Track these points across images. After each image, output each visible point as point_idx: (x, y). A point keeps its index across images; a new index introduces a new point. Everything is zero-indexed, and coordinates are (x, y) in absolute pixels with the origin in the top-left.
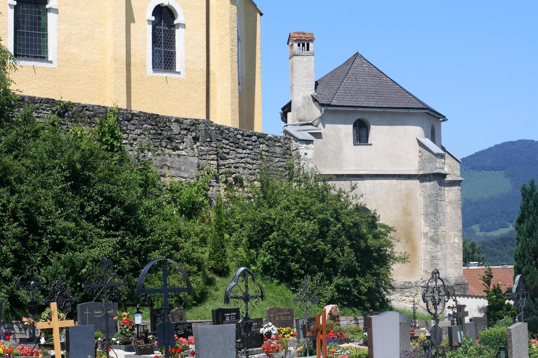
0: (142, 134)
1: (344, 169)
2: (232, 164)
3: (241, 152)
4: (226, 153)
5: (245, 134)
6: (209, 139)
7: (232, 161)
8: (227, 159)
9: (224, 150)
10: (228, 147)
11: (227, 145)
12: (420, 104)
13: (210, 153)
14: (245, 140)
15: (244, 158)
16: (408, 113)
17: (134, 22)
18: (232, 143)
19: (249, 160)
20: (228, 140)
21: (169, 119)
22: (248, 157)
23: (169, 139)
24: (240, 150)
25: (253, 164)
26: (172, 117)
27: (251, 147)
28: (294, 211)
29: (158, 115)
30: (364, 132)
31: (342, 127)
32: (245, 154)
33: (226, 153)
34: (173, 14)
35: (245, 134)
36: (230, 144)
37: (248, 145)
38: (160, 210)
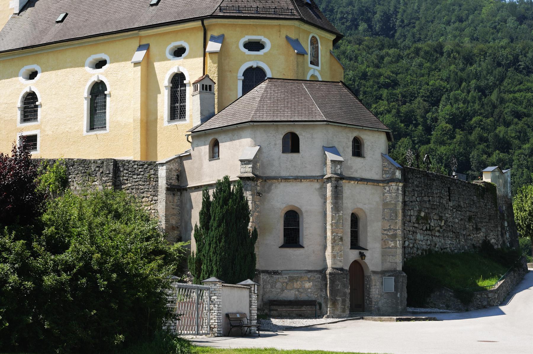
1: (203, 181)
2: (130, 187)
4: (125, 180)
5: (139, 164)
6: (108, 172)
7: (129, 185)
8: (126, 184)
9: (125, 178)
10: (127, 175)
11: (126, 173)
13: (107, 181)
14: (139, 168)
15: (137, 181)
16: (261, 125)
17: (160, 93)
18: (130, 172)
19: (140, 183)
20: (128, 170)
21: (90, 161)
22: (140, 181)
23: (89, 175)
24: (135, 177)
25: (144, 185)
26: (92, 160)
27: (142, 173)
29: (86, 160)
30: (216, 149)
31: (203, 148)
32: (139, 178)
33: (125, 180)
34: (174, 77)
35: (139, 164)
36: (130, 173)
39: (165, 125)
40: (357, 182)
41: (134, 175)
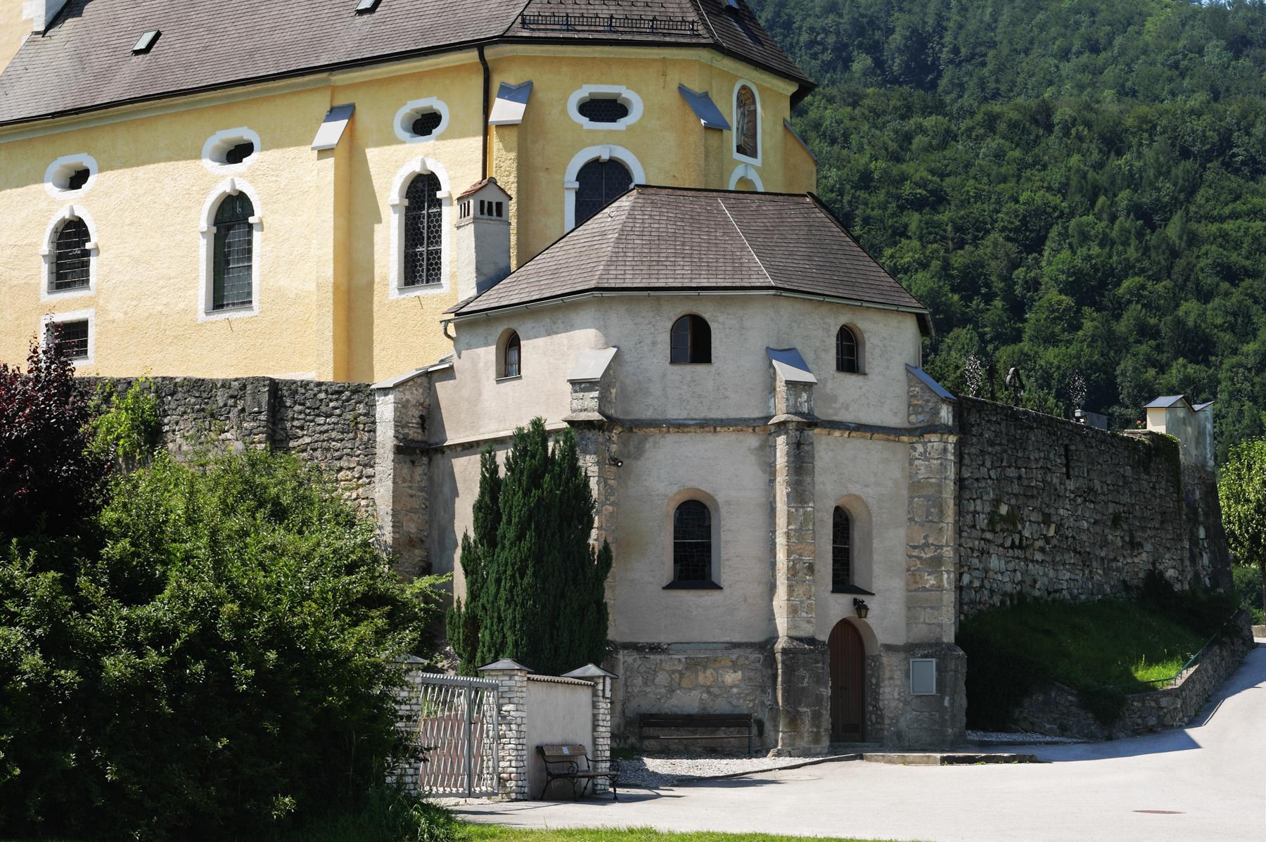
0: (185, 413)
1: (481, 431)
2: (308, 444)
3: (322, 422)
4: (297, 427)
5: (330, 391)
6: (256, 409)
7: (307, 440)
8: (299, 438)
9: (296, 423)
10: (302, 416)
11: (300, 413)
12: (566, 680)
13: (255, 431)
14: (331, 401)
15: (326, 431)
16: (621, 297)
18: (308, 408)
19: (334, 434)
20: (303, 404)
21: (213, 383)
22: (333, 430)
23: (212, 415)
24: (321, 420)
25: (342, 440)
26: (218, 380)
27: (338, 412)
28: (1020, 100)
30: (514, 355)
31: (481, 351)
32: (329, 424)
33: (297, 427)
34: (413, 182)
35: (330, 391)
36: (308, 411)
37: (335, 408)
38: (1120, 163)
39: (391, 298)
41: (318, 415)
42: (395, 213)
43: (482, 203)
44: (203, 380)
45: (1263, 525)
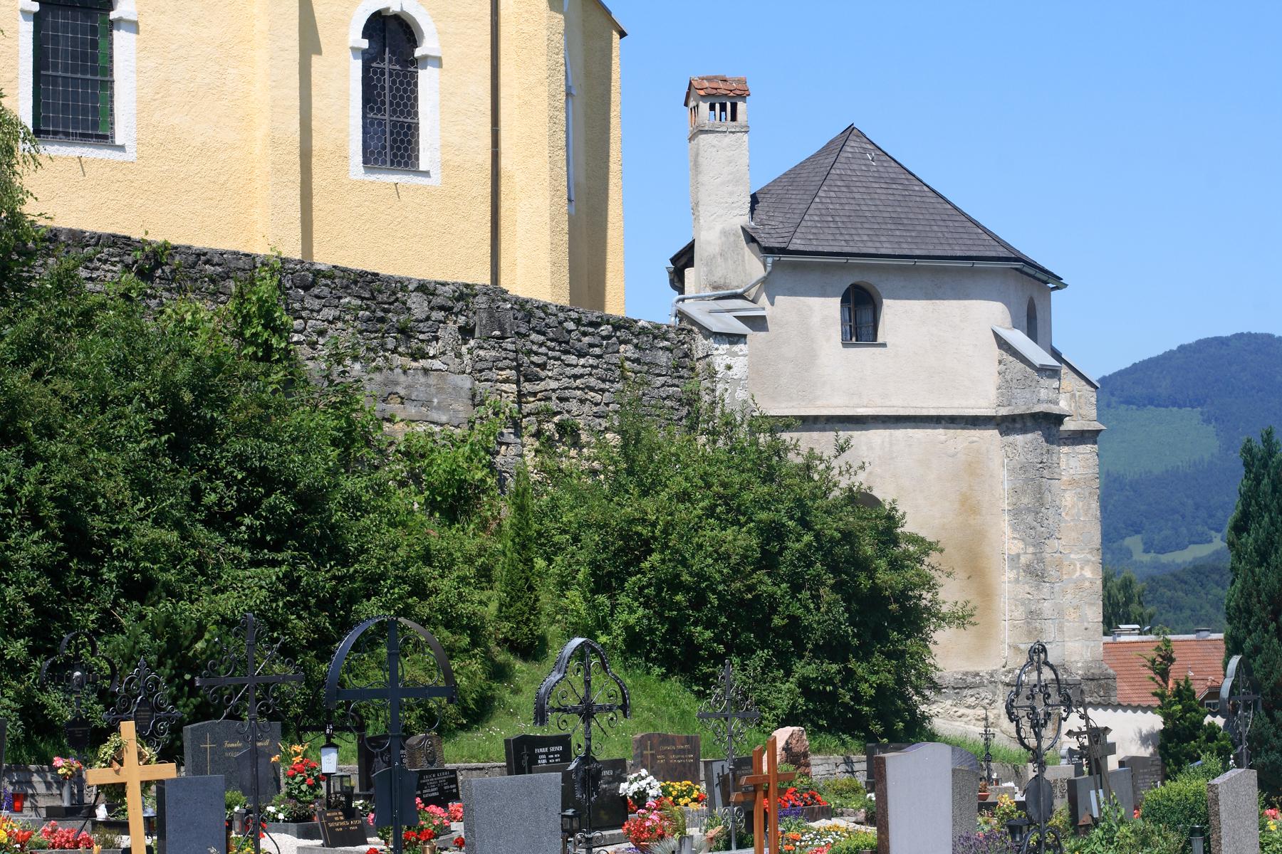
1: (819, 403)
2: (554, 390)
4: (538, 365)
5: (584, 321)
6: (497, 333)
7: (554, 385)
8: (542, 380)
9: (535, 359)
10: (543, 350)
11: (541, 345)
13: (500, 365)
14: (585, 334)
15: (582, 376)
16: (972, 269)
18: (552, 340)
19: (593, 382)
20: (544, 334)
21: (402, 284)
22: (590, 374)
23: (402, 331)
24: (572, 359)
25: (603, 391)
26: (409, 280)
27: (597, 351)
30: (866, 315)
31: (815, 303)
32: (583, 366)
33: (538, 365)
34: (412, 34)
35: (584, 321)
36: (549, 343)
39: (352, 176)
40: (505, 764)
41: (566, 352)
42: (355, 58)
43: (734, 118)
44: (376, 275)
45: (5, 516)
